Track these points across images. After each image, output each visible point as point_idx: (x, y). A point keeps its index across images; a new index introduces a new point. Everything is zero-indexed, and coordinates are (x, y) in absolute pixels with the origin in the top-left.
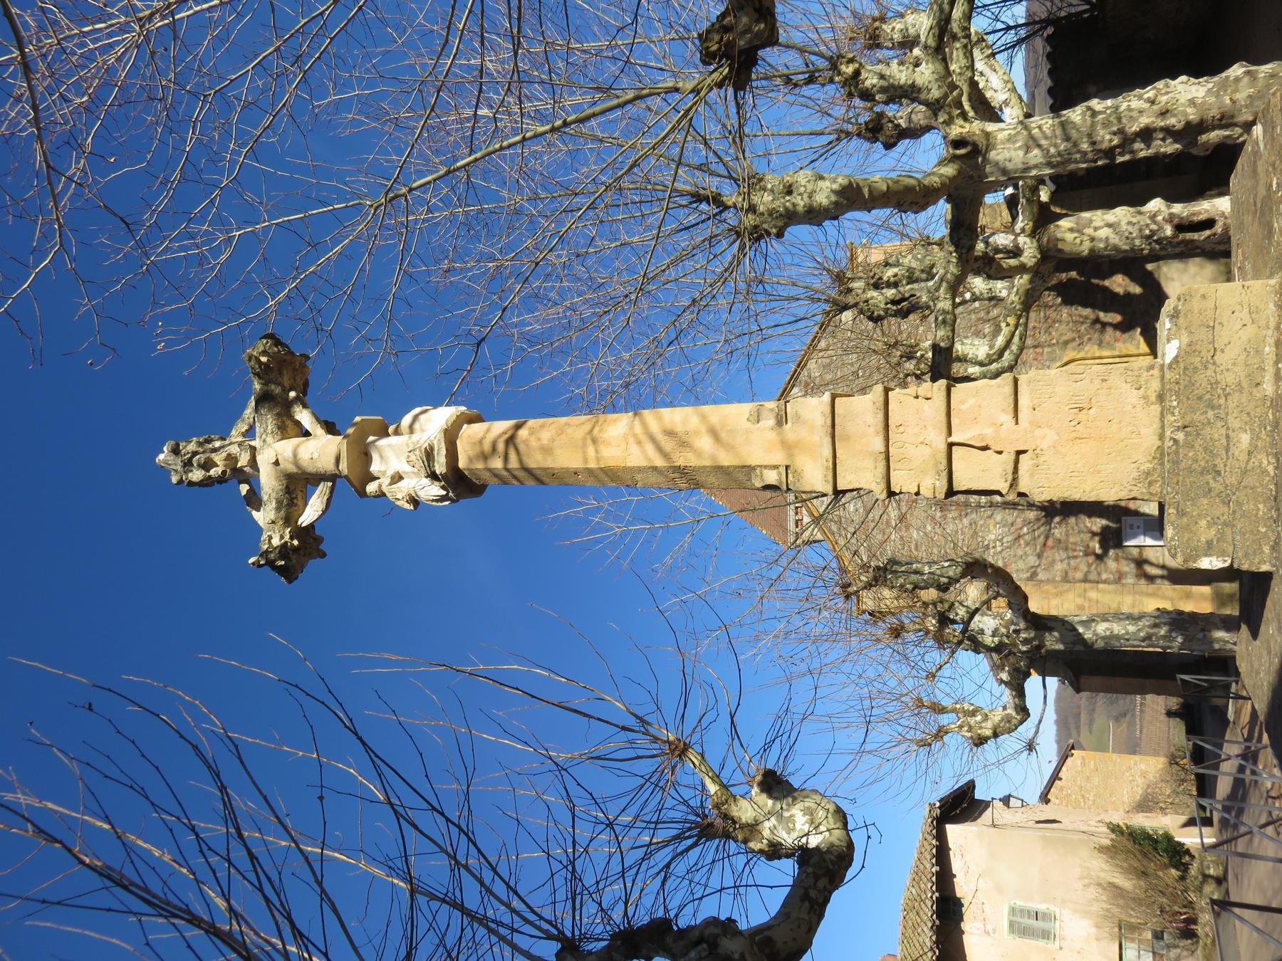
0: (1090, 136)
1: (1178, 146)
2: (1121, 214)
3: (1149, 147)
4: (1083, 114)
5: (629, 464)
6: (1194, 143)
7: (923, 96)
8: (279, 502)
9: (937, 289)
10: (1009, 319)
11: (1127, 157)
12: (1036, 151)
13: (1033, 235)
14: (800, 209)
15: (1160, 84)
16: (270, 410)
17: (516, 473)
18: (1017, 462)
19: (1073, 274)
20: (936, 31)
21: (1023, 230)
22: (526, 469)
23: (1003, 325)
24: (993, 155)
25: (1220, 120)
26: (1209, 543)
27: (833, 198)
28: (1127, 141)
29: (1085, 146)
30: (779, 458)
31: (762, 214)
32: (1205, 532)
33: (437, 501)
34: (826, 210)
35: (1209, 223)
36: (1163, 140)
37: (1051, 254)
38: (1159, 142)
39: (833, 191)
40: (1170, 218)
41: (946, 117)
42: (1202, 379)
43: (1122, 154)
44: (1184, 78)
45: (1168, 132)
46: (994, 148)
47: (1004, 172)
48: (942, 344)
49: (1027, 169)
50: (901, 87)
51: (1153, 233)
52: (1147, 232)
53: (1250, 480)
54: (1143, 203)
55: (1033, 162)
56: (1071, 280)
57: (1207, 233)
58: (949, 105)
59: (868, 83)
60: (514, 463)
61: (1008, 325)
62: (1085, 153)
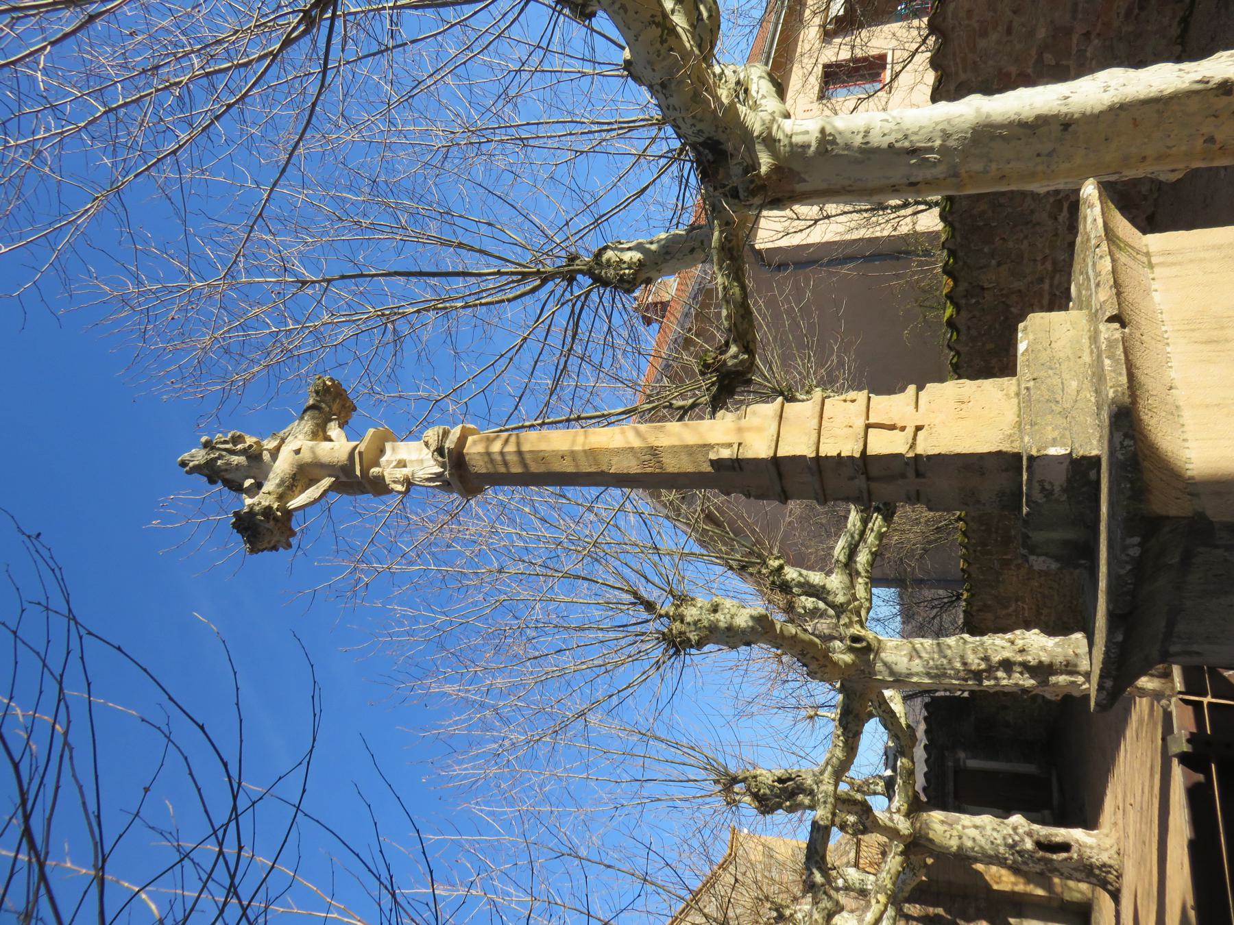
0: (962, 657)
1: (1032, 682)
2: (986, 820)
3: (1010, 677)
4: (957, 641)
5: (611, 446)
6: (1044, 682)
7: (830, 598)
8: (282, 482)
9: (822, 773)
10: (879, 896)
11: (992, 682)
12: (917, 661)
13: (907, 815)
14: (722, 625)
15: (1018, 632)
16: (313, 418)
17: (508, 458)
18: (915, 435)
19: (940, 911)
20: (847, 551)
21: (899, 810)
22: (520, 453)
23: (873, 901)
24: (883, 655)
25: (1067, 666)
26: (1054, 440)
27: (750, 624)
28: (991, 670)
29: (958, 665)
30: (733, 439)
31: (689, 624)
32: (1050, 433)
33: (428, 480)
34: (744, 631)
35: (1065, 847)
36: (1021, 673)
37: (922, 842)
38: (1018, 675)
39: (752, 617)
40: (1030, 834)
41: (847, 620)
42: (1044, 356)
43: (988, 678)
44: (1037, 631)
45: (1025, 666)
46: (884, 650)
47: (892, 673)
48: (821, 823)
49: (910, 675)
50: (814, 586)
51: (1015, 844)
52: (1010, 841)
53: (1079, 405)
54: (1007, 818)
55: (915, 670)
56: (937, 915)
57: (1064, 855)
58: (851, 611)
59: (788, 577)
60: (511, 448)
61: (878, 902)
62: (959, 671)
